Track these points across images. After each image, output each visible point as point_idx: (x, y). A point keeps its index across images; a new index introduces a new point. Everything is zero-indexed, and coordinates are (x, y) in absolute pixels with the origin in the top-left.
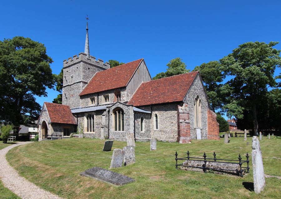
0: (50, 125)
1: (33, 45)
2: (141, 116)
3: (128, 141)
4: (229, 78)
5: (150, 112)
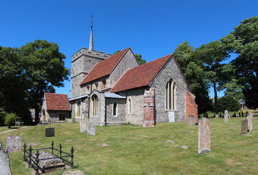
0: (47, 112)
1: (48, 46)
2: (114, 102)
3: (81, 126)
4: (234, 56)
5: (125, 97)
